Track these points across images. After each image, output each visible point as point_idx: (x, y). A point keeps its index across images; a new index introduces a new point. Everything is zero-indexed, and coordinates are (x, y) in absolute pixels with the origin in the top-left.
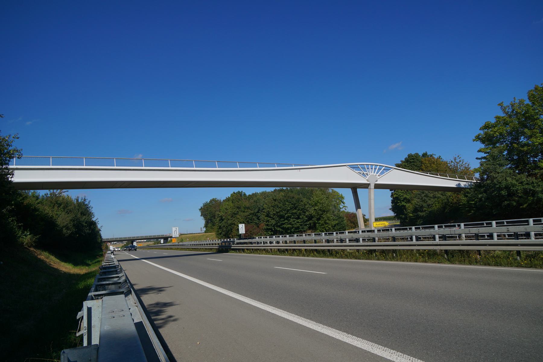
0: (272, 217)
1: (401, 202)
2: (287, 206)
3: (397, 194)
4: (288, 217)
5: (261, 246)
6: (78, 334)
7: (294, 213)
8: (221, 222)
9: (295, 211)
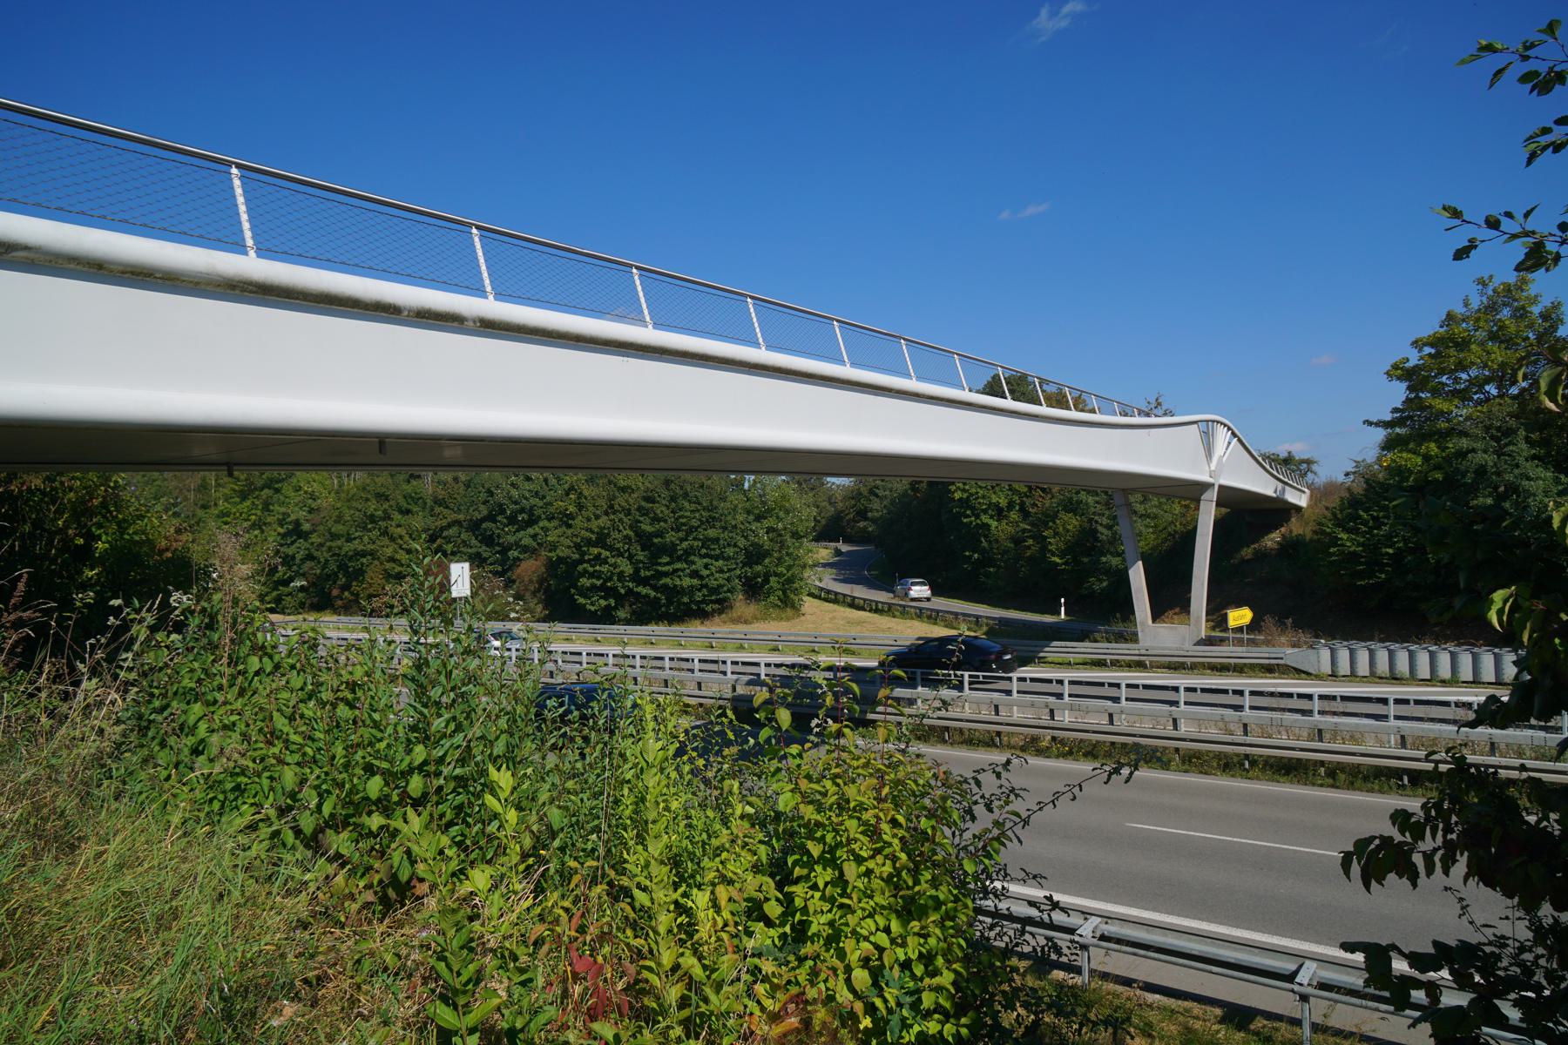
0: (618, 549)
1: (977, 516)
2: (688, 514)
3: (964, 491)
4: (689, 552)
5: (1050, 660)
6: (1466, 854)
7: (710, 540)
8: (292, 543)
9: (712, 533)
